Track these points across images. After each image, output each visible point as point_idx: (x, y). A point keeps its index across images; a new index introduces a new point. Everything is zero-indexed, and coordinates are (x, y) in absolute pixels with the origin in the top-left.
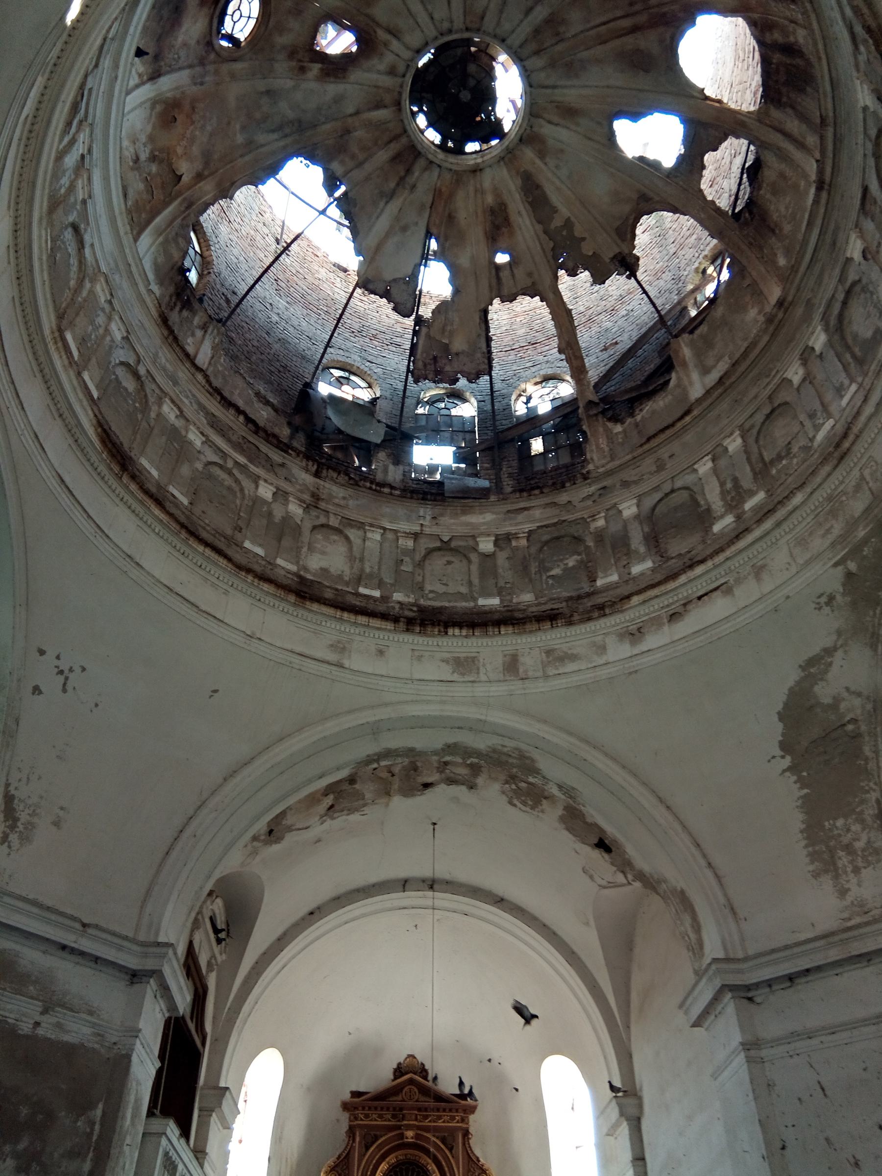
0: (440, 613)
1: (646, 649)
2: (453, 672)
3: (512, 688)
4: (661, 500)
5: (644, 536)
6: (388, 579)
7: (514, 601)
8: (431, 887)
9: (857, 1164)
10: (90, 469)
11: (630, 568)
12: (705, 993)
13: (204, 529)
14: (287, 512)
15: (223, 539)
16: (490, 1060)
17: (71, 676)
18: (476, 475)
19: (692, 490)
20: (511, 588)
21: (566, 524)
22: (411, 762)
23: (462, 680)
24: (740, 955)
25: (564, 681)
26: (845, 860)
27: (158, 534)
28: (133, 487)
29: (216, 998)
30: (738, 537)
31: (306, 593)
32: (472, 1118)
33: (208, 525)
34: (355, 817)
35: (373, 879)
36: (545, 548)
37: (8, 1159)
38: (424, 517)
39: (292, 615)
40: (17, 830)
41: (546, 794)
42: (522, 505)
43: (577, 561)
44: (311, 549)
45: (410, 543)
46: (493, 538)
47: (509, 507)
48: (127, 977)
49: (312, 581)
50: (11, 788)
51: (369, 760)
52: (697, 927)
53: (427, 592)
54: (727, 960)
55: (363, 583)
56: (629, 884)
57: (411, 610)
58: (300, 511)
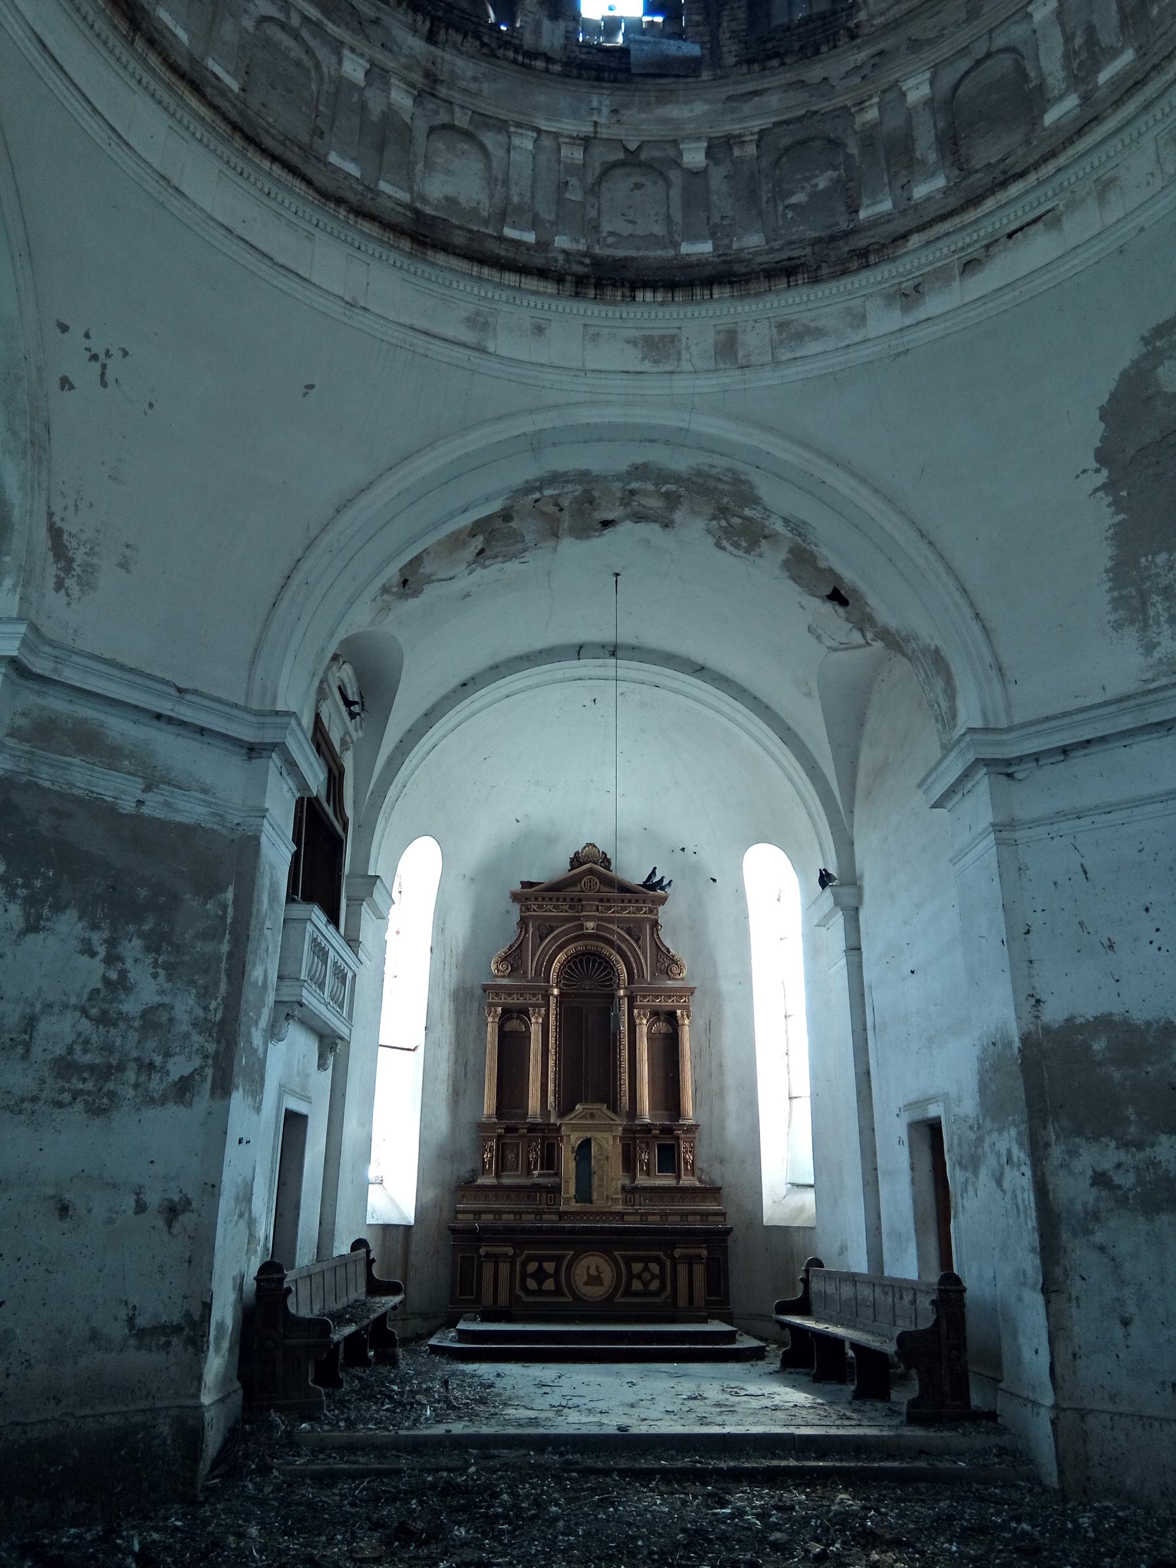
0: (624, 267)
1: (924, 317)
2: (643, 359)
3: (727, 380)
4: (967, 73)
5: (936, 135)
6: (547, 213)
7: (735, 246)
8: (613, 654)
9: (1111, 947)
10: (82, 25)
11: (911, 191)
12: (954, 768)
13: (267, 131)
14: (389, 105)
15: (296, 149)
16: (683, 849)
17: (108, 362)
18: (680, 35)
19: (1018, 53)
20: (730, 226)
21: (816, 118)
22: (586, 491)
23: (658, 370)
24: (1004, 724)
25: (800, 369)
26: (1160, 607)
27: (201, 141)
28: (153, 60)
29: (355, 780)
30: (1080, 132)
31: (425, 236)
32: (661, 908)
33: (273, 127)
34: (513, 566)
35: (539, 645)
36: (784, 160)
37: (133, 939)
38: (599, 111)
39: (408, 271)
40: (73, 573)
41: (767, 532)
42: (750, 87)
43: (831, 179)
44: (429, 166)
45: (578, 155)
46: (705, 144)
47: (731, 90)
48: (244, 751)
49: (434, 217)
50: (56, 519)
51: (528, 489)
52: (951, 692)
53: (604, 234)
54: (986, 730)
55: (509, 220)
56: (868, 644)
57: (581, 263)
58: (408, 102)
